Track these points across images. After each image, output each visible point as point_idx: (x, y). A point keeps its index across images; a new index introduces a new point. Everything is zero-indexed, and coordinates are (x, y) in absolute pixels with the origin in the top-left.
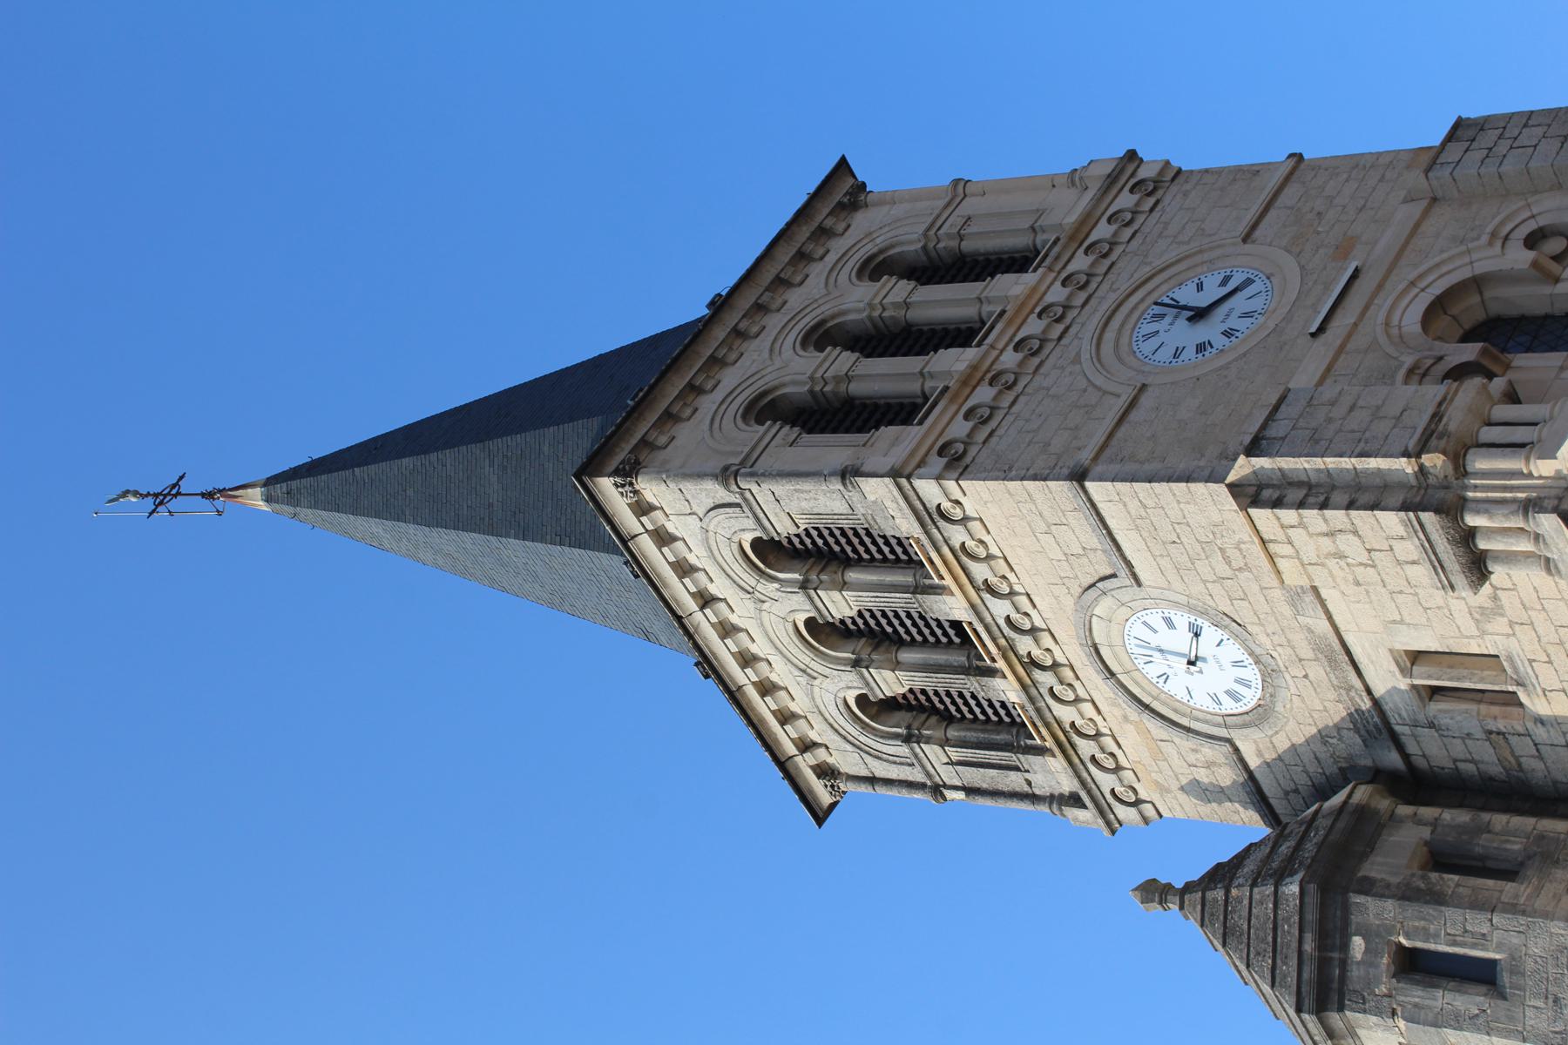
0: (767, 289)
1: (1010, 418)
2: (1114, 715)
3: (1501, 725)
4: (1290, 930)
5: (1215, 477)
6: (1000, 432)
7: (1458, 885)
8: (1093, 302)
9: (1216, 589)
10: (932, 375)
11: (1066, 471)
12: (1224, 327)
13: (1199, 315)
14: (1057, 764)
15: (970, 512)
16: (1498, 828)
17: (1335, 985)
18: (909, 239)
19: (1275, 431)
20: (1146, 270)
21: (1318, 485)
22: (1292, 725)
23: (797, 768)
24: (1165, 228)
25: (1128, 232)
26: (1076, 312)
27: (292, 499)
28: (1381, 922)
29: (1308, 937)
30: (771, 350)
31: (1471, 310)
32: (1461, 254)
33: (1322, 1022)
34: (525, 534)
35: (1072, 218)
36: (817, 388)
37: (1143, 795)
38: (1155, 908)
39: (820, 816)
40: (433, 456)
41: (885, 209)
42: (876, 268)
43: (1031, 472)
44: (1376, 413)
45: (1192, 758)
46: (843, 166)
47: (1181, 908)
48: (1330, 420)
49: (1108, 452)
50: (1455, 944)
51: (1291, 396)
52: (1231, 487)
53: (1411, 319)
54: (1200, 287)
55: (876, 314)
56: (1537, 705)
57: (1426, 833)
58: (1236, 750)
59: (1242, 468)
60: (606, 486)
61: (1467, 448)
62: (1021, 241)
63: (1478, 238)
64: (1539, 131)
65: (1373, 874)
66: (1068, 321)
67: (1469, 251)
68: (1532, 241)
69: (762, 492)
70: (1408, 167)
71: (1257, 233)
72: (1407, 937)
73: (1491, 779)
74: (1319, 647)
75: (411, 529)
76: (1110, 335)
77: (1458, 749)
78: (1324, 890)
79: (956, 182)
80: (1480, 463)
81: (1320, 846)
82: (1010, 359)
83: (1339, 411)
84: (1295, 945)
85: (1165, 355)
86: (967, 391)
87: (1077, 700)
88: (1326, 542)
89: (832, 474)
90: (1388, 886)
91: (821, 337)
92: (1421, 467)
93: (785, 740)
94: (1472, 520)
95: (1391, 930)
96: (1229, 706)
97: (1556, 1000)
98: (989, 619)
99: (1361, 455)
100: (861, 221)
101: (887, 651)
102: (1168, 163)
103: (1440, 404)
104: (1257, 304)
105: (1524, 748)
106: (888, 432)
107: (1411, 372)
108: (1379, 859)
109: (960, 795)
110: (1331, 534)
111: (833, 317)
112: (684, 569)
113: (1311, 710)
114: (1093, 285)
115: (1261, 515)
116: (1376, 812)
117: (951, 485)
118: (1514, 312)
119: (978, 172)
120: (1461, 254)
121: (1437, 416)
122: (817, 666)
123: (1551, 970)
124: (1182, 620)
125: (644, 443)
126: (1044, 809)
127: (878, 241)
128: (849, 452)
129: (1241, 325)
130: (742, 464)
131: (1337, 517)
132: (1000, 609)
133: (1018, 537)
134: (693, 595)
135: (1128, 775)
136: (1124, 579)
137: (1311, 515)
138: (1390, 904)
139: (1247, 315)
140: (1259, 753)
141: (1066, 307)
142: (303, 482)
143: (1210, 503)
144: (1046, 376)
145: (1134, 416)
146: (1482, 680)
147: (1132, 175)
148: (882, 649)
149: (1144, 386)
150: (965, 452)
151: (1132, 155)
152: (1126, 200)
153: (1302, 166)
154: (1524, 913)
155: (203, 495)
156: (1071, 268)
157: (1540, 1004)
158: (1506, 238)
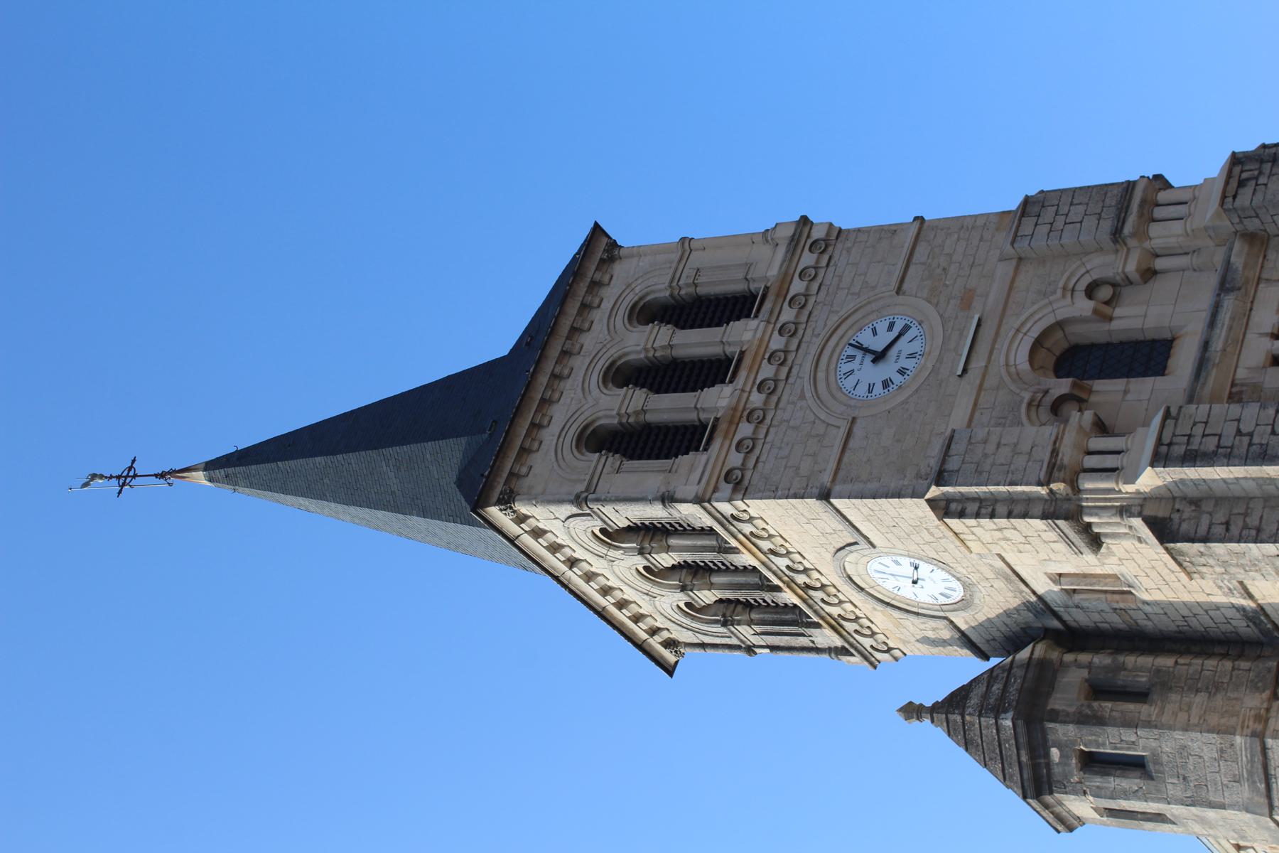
0: (568, 338)
1: (767, 446)
2: (866, 607)
3: (1122, 605)
4: (1010, 748)
5: (915, 495)
6: (763, 458)
7: (1112, 710)
8: (803, 345)
9: (926, 547)
10: (703, 410)
11: (816, 491)
12: (898, 366)
13: (879, 357)
14: (828, 631)
15: (753, 514)
16: (1130, 666)
17: (1045, 779)
18: (660, 288)
19: (953, 464)
20: (834, 319)
21: (986, 500)
22: (986, 609)
23: (650, 645)
24: (840, 281)
25: (815, 286)
26: (793, 355)
27: (229, 480)
28: (1066, 740)
29: (1023, 753)
30: (583, 389)
31: (1059, 343)
32: (1045, 306)
33: (1040, 802)
34: (424, 513)
35: (774, 272)
36: (624, 421)
37: (891, 645)
38: (915, 723)
39: (670, 670)
40: (340, 457)
41: (635, 260)
42: (647, 313)
43: (792, 492)
44: (1015, 451)
45: (922, 627)
46: (597, 229)
47: (933, 721)
48: (986, 456)
49: (841, 474)
50: (1116, 748)
51: (956, 436)
52: (928, 501)
53: (1021, 357)
54: (875, 332)
55: (650, 354)
56: (1146, 597)
57: (1085, 673)
58: (952, 622)
59: (934, 492)
60: (494, 512)
61: (1077, 474)
62: (739, 287)
63: (1054, 292)
64: (1081, 208)
65: (1057, 707)
66: (789, 362)
67: (1050, 303)
68: (1090, 292)
69: (608, 510)
70: (997, 229)
71: (905, 286)
72: (1085, 745)
73: (1120, 630)
74: (999, 574)
75: (333, 505)
76: (821, 375)
77: (1097, 617)
78: (1028, 723)
79: (683, 239)
80: (1088, 484)
81: (1020, 691)
82: (757, 399)
83: (991, 448)
84: (1015, 757)
85: (862, 390)
86: (733, 427)
87: (841, 602)
88: (998, 534)
89: (655, 499)
90: (1068, 714)
91: (623, 375)
92: (1051, 490)
93: (640, 632)
94: (1087, 519)
95: (1074, 743)
96: (943, 600)
97: (1185, 778)
98: (775, 568)
99: (1010, 484)
100: (620, 271)
101: (703, 577)
102: (831, 225)
103: (1055, 443)
104: (916, 347)
105: (1139, 617)
106: (684, 460)
107: (1029, 405)
108: (1058, 696)
110: (1000, 530)
111: (620, 358)
112: (555, 548)
113: (996, 602)
114: (800, 332)
115: (954, 523)
116: (1050, 662)
117: (739, 504)
118: (1087, 342)
119: (699, 231)
120: (1045, 306)
121: (1055, 452)
122: (655, 590)
123: (1179, 760)
124: (906, 562)
125: (512, 474)
126: (825, 656)
127: (637, 290)
128: (661, 477)
129: (910, 364)
130: (587, 490)
131: (1003, 522)
132: (782, 563)
133: (790, 530)
134: (563, 562)
135: (881, 637)
137: (985, 522)
138: (1071, 727)
139: (911, 356)
140: (967, 622)
141: (786, 352)
142: (235, 466)
143: (916, 510)
144: (784, 410)
145: (851, 444)
146: (1106, 585)
147: (808, 236)
148: (699, 576)
149: (854, 419)
150: (743, 476)
151: (804, 220)
152: (808, 259)
153: (926, 225)
154: (1156, 727)
155: (156, 476)
156: (783, 319)
157: (1175, 781)
158: (1073, 290)
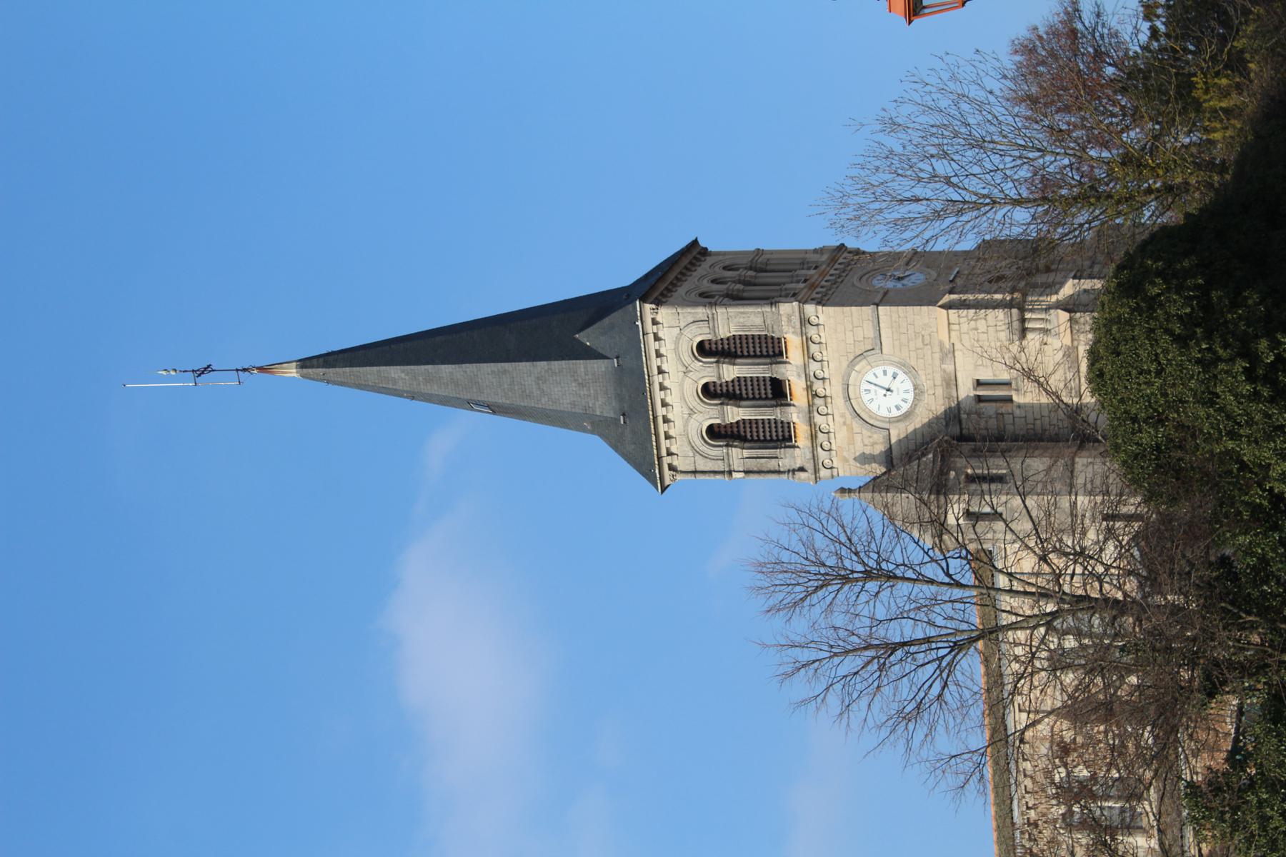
3: (1003, 410)
13: (899, 279)
59: (947, 298)
109: (742, 475)
136: (878, 351)
